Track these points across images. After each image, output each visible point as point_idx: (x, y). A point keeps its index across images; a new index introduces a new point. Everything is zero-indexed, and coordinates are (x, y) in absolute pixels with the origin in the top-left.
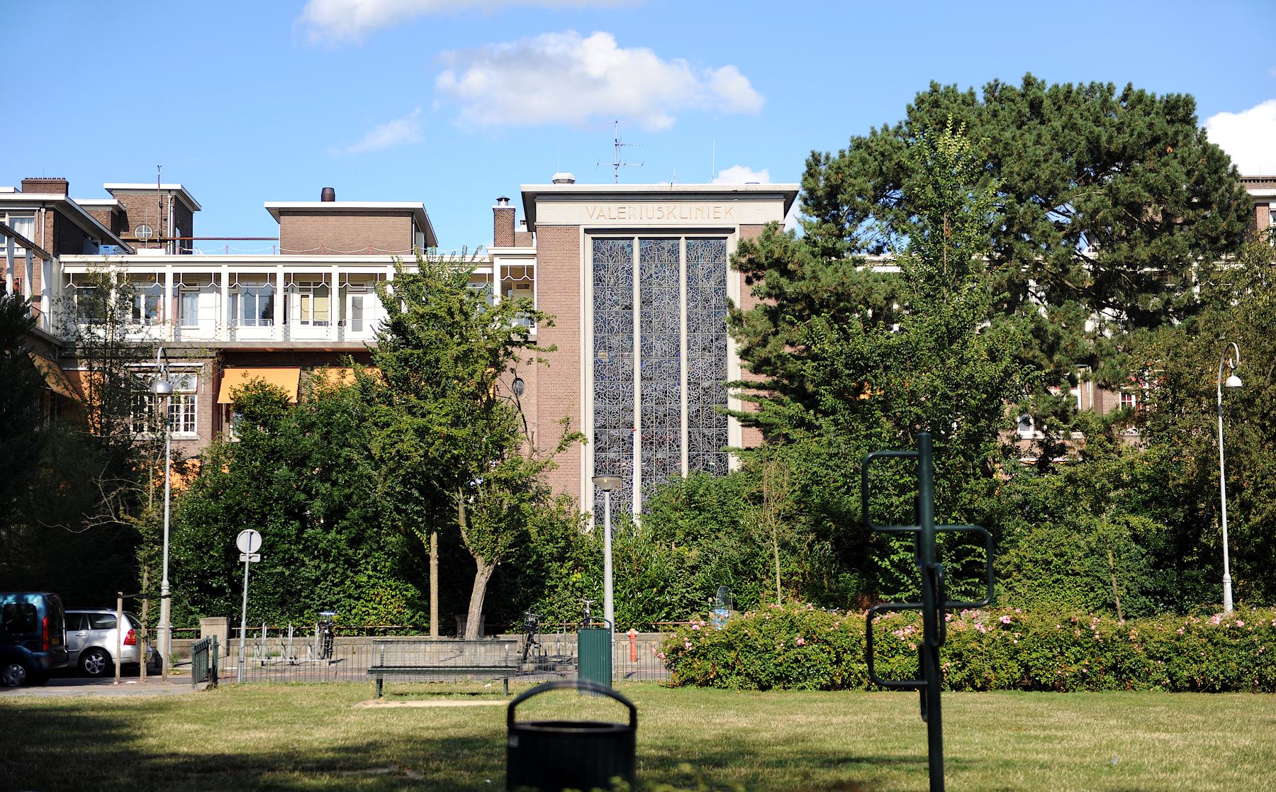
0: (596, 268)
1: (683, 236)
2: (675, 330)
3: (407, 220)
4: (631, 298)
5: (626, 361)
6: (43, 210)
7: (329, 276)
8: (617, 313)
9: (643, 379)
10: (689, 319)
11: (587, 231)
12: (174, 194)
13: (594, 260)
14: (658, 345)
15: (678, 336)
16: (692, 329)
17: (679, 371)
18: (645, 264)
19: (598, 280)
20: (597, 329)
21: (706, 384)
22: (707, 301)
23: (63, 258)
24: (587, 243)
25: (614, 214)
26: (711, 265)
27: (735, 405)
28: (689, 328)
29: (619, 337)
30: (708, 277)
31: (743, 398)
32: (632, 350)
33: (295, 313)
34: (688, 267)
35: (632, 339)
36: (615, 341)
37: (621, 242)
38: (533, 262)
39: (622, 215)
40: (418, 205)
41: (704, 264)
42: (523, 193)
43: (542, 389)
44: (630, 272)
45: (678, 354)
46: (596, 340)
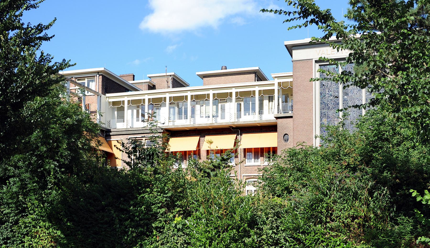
3: (253, 75)
4: (338, 92)
6: (98, 75)
8: (331, 100)
11: (316, 62)
12: (172, 77)
23: (108, 95)
33: (197, 112)
38: (291, 80)
40: (257, 68)
42: (286, 46)
43: (295, 137)
46: (321, 113)
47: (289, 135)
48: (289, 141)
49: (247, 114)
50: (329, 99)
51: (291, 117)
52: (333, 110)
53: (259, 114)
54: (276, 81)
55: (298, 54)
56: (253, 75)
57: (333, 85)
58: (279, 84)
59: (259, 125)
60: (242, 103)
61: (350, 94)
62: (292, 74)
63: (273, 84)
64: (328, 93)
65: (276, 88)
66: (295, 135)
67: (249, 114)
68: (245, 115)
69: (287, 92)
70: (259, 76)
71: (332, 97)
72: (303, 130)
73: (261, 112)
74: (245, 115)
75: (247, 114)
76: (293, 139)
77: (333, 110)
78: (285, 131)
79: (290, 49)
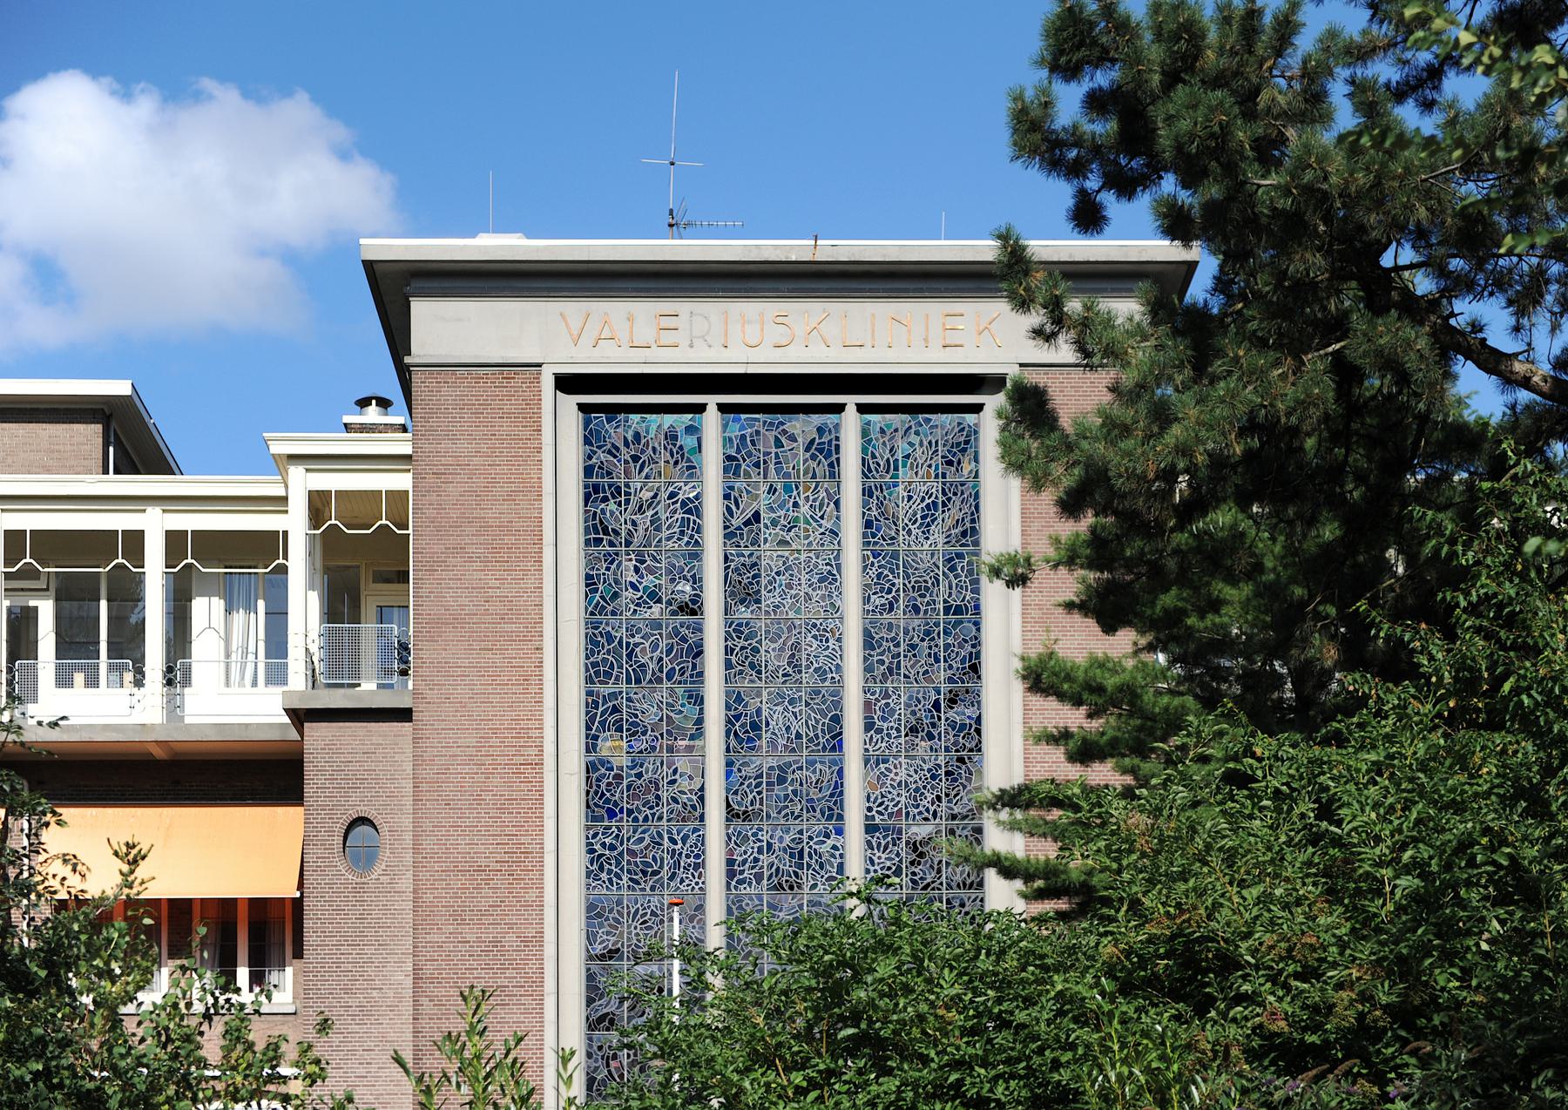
0: (591, 494)
1: (851, 400)
2: (831, 672)
3: (90, 434)
4: (697, 581)
5: (682, 764)
7: (135, 541)
8: (656, 624)
9: (731, 814)
10: (869, 642)
11: (566, 383)
13: (588, 471)
14: (777, 718)
15: (839, 684)
16: (880, 668)
17: (838, 791)
18: (740, 484)
19: (597, 531)
20: (596, 672)
21: (921, 831)
22: (922, 590)
24: (563, 420)
25: (645, 333)
26: (936, 487)
27: (1000, 839)
28: (868, 669)
29: (663, 691)
30: (927, 519)
31: (1013, 826)
32: (699, 733)
34: (867, 492)
35: (699, 700)
36: (652, 704)
37: (668, 420)
38: (401, 481)
39: (667, 338)
40: (121, 388)
41: (914, 484)
42: (369, 266)
43: (427, 844)
44: (693, 508)
45: (836, 742)
47: (384, 829)
48: (379, 868)
49: (79, 678)
50: (627, 618)
51: (404, 715)
52: (666, 684)
53: (170, 683)
54: (301, 483)
55: (440, 326)
56: (90, 434)
57: (665, 534)
58: (318, 503)
59: (159, 753)
60: (46, 610)
61: (768, 600)
62: (407, 449)
63: (279, 503)
64: (632, 577)
65: (295, 524)
66: (427, 825)
67: (92, 682)
68: (64, 681)
69: (364, 562)
70: (130, 440)
71: (656, 609)
72: (479, 799)
73: (176, 676)
74: (64, 681)
75: (79, 678)
76: (416, 849)
77: (666, 684)
78: (354, 799)
79: (394, 289)
